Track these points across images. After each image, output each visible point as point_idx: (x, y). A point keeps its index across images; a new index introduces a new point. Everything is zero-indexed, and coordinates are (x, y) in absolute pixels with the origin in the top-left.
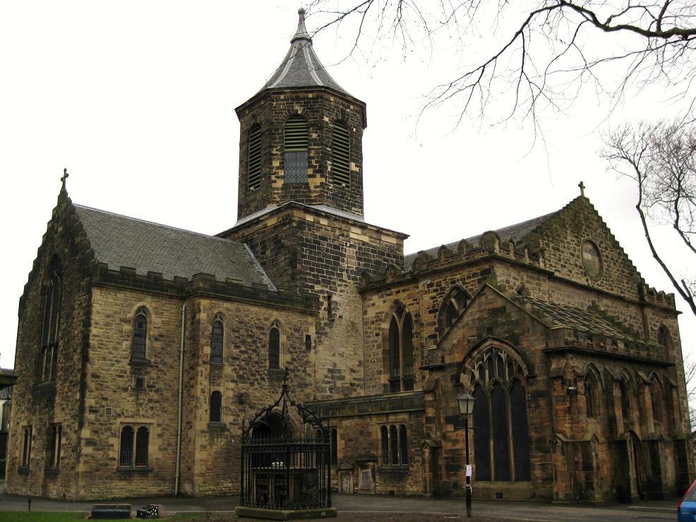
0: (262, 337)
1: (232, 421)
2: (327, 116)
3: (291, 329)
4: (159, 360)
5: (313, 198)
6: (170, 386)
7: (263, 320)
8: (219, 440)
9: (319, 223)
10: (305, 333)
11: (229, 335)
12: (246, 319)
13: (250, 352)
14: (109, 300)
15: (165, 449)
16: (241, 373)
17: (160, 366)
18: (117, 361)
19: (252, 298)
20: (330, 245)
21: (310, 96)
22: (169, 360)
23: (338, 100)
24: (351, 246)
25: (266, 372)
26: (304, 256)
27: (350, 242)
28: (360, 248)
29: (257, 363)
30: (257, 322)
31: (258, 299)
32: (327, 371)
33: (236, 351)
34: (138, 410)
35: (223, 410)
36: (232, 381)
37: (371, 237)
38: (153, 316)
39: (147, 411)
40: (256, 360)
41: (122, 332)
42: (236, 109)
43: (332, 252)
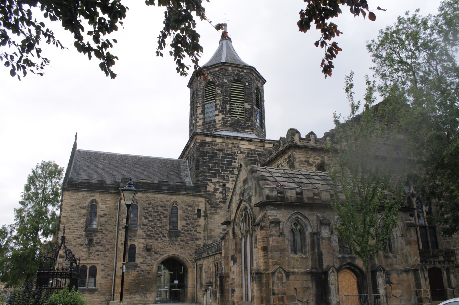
0: (164, 211)
1: (142, 262)
2: (226, 79)
3: (185, 206)
4: (103, 228)
5: (218, 128)
6: (110, 242)
7: (165, 202)
8: (133, 272)
9: (216, 141)
10: (196, 208)
11: (141, 212)
12: (153, 202)
13: (155, 221)
14: (74, 197)
15: (106, 278)
16: (149, 233)
17: (104, 231)
18: (77, 230)
19: (157, 189)
20: (225, 154)
21: (217, 69)
22: (109, 228)
23: (234, 68)
24: (241, 153)
25: (166, 232)
26: (205, 162)
27: (240, 150)
28: (248, 153)
29: (160, 227)
30: (161, 203)
31: (161, 190)
32: (221, 230)
33: (145, 221)
34: (89, 256)
35: (137, 255)
36: (142, 238)
37: (257, 146)
38: (100, 204)
39: (94, 256)
40: (160, 225)
41: (80, 214)
42: (188, 86)
43: (226, 158)
